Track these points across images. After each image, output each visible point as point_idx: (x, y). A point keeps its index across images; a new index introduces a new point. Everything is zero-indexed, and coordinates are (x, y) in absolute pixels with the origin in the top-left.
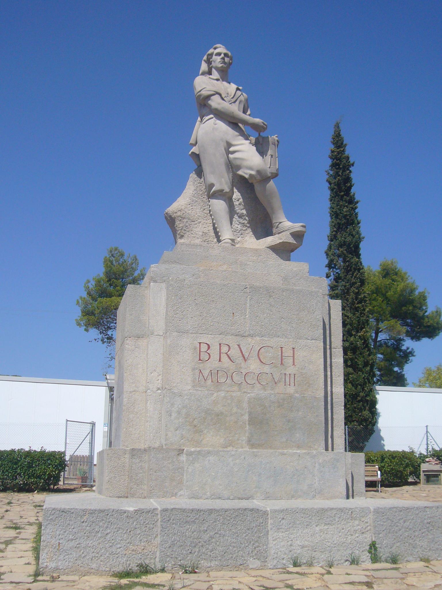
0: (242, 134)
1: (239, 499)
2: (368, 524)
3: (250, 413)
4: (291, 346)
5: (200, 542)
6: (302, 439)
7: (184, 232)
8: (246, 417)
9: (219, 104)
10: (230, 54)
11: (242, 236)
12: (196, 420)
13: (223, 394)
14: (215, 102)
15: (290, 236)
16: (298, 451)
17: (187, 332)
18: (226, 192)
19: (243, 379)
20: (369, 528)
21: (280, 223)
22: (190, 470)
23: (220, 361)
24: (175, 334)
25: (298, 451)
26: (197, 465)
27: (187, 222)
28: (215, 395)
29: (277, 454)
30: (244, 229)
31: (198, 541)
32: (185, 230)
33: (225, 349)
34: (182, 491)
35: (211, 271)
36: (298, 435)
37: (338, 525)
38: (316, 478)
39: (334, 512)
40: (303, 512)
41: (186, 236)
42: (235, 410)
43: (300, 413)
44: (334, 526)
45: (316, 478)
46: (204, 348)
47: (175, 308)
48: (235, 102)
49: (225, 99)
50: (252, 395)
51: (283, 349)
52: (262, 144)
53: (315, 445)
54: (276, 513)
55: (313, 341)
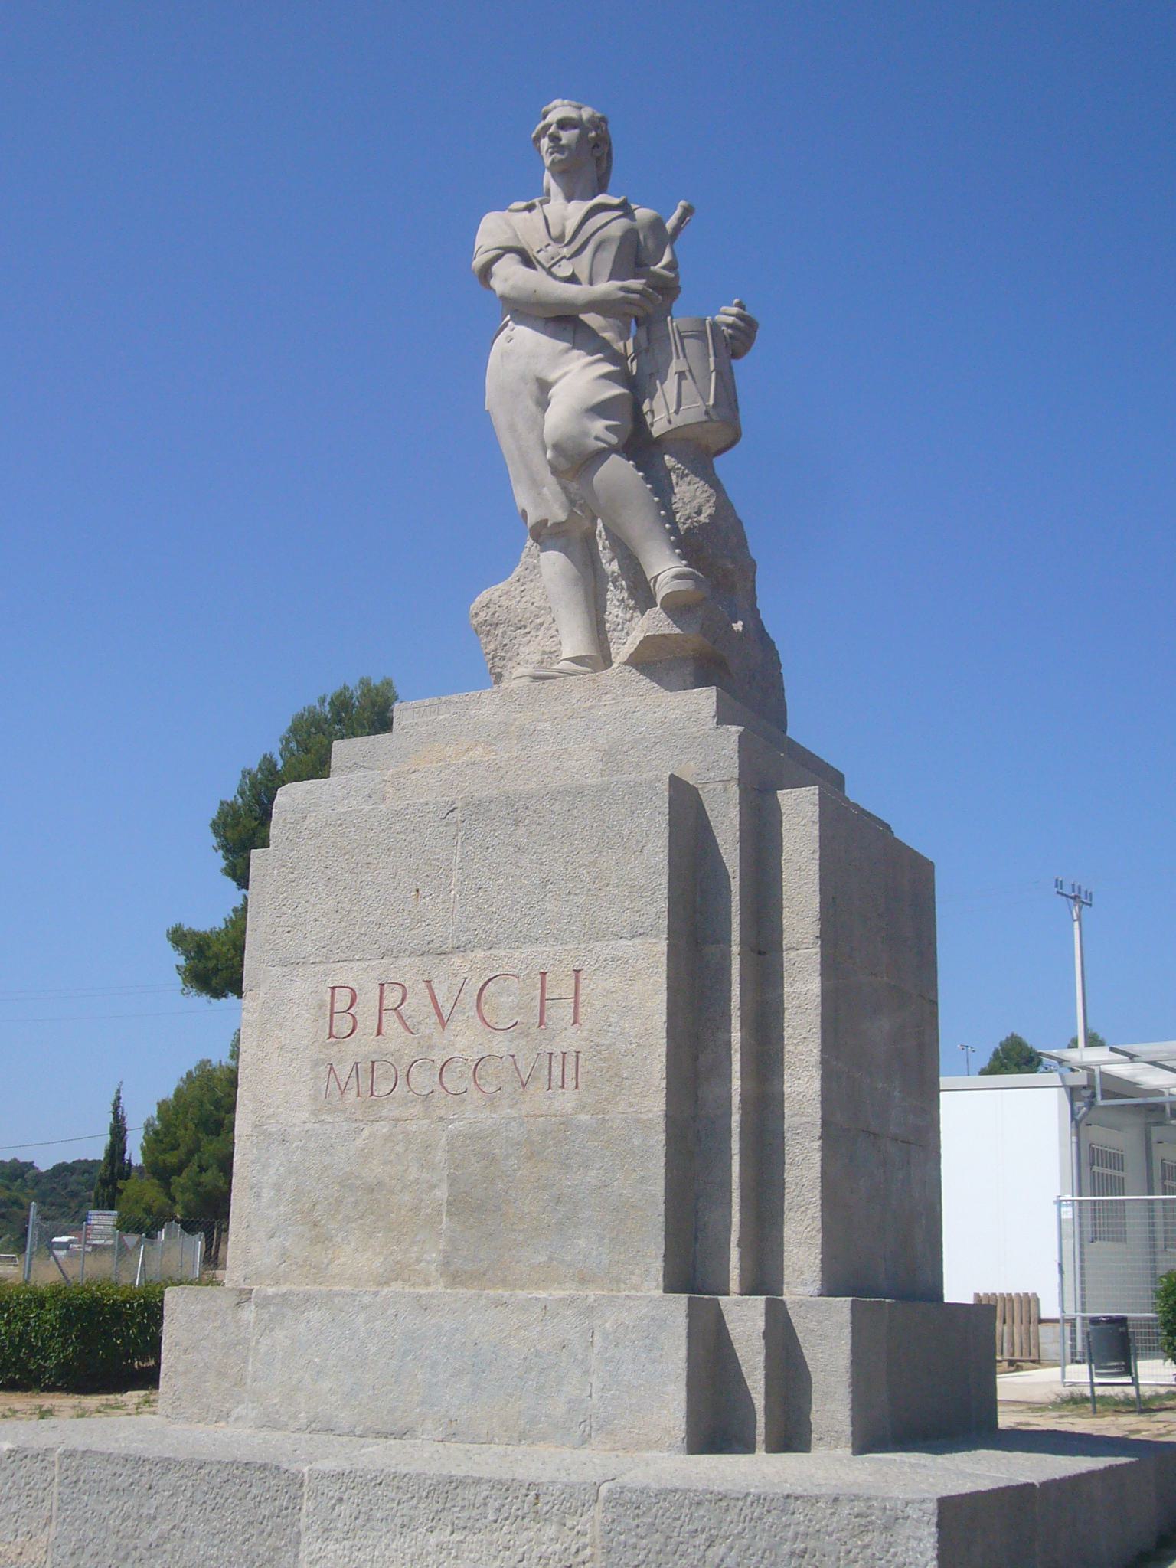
1: (379, 1434)
2: (587, 1540)
3: (453, 1181)
4: (571, 967)
5: (135, 1548)
6: (594, 1253)
7: (499, 663)
8: (442, 1193)
12: (318, 1207)
13: (384, 1128)
16: (542, 1294)
17: (302, 962)
18: (558, 524)
19: (437, 1079)
20: (588, 1552)
21: (656, 578)
22: (263, 1348)
23: (379, 1033)
24: (277, 971)
25: (542, 1294)
26: (280, 1334)
27: (504, 633)
28: (365, 1133)
29: (483, 1302)
31: (131, 1546)
32: (503, 658)
33: (392, 997)
34: (241, 1407)
35: (413, 776)
36: (582, 1243)
37: (492, 1532)
38: (594, 1379)
39: (484, 1490)
40: (395, 1482)
41: (506, 674)
42: (413, 1173)
43: (593, 1173)
44: (479, 1536)
45: (594, 1379)
46: (343, 999)
47: (278, 902)
50: (459, 1126)
51: (548, 977)
52: (647, 350)
53: (632, 1273)
54: (325, 1481)
55: (637, 941)
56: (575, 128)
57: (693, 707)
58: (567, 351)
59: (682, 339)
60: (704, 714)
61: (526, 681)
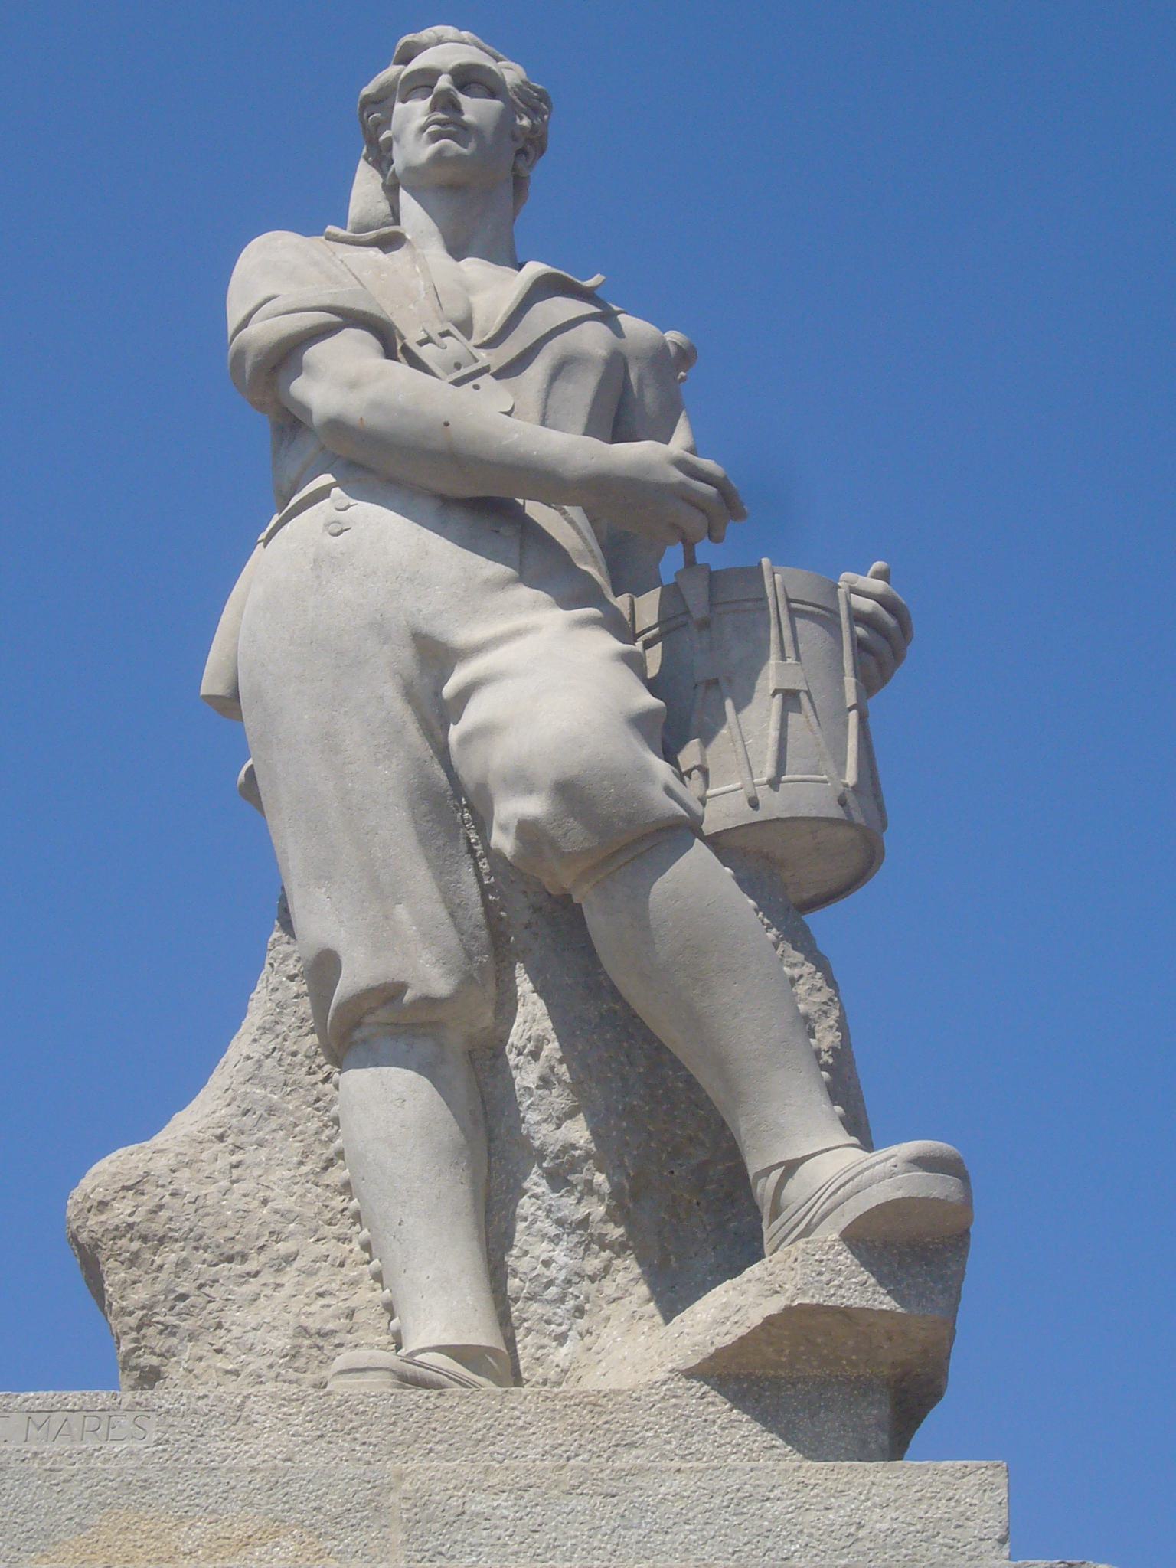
0: (539, 564)
7: (160, 1343)
9: (354, 385)
10: (512, 73)
11: (582, 1324)
14: (341, 381)
15: (847, 1258)
18: (428, 1002)
21: (791, 1167)
27: (183, 1264)
30: (593, 1264)
32: (169, 1330)
41: (174, 1372)
48: (510, 370)
49: (426, 353)
52: (705, 625)
56: (492, 95)
57: (942, 1509)
58: (504, 584)
59: (793, 613)
60: (974, 1529)
61: (378, 1384)
